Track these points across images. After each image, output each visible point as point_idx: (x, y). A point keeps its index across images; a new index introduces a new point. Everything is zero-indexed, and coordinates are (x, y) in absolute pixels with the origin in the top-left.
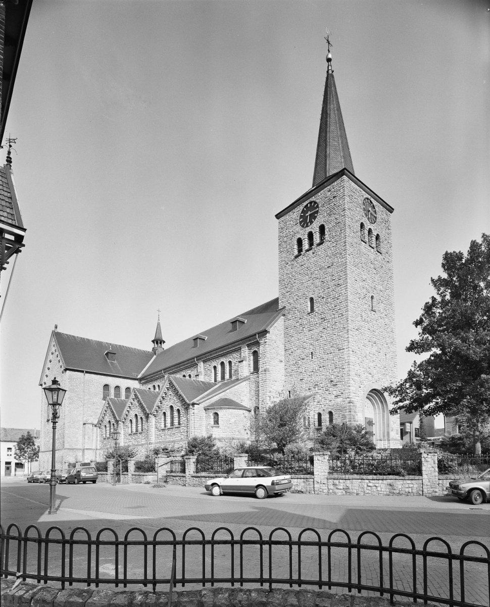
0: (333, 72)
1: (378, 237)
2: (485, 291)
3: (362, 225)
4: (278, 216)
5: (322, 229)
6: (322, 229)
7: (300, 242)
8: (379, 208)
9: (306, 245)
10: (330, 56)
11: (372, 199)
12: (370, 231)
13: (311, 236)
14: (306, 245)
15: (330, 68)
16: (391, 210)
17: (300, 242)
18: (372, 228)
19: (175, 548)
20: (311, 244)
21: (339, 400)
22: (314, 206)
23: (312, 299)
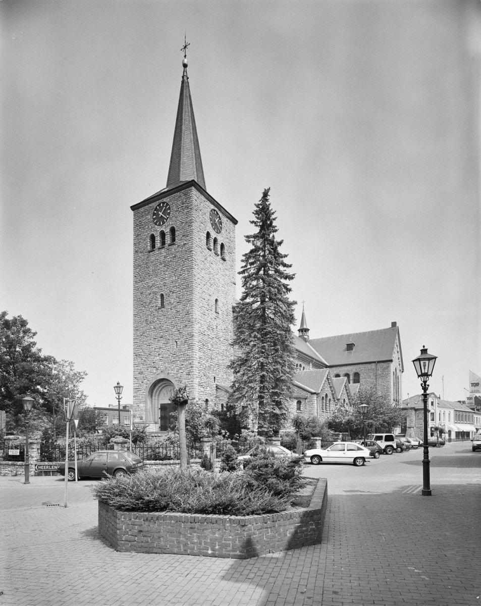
0: (188, 78)
1: (222, 246)
2: (228, 413)
3: (208, 235)
4: (134, 208)
5: (173, 230)
6: (173, 230)
7: (153, 238)
8: (224, 219)
9: (158, 244)
10: (186, 61)
11: (219, 212)
12: (215, 240)
13: (163, 234)
14: (158, 244)
15: (185, 74)
16: (235, 222)
17: (153, 238)
18: (218, 238)
19: (420, 445)
20: (163, 243)
21: (198, 240)
22: (167, 208)
23: (162, 296)
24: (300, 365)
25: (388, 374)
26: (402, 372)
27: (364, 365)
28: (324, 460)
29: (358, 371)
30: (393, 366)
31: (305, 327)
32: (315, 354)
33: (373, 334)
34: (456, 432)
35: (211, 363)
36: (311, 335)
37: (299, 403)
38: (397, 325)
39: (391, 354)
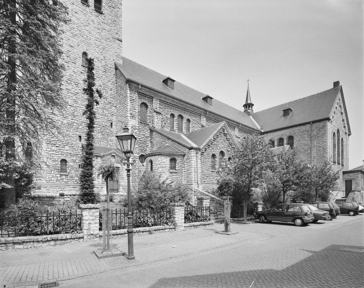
4: (283, 110)
24: (181, 117)
25: (325, 134)
26: (349, 135)
27: (298, 128)
28: (147, 233)
29: (292, 134)
30: (331, 128)
31: (249, 102)
32: (256, 126)
33: (313, 97)
34: (99, 231)
35: (73, 121)
36: (256, 109)
37: (173, 160)
38: (340, 84)
39: (329, 112)
